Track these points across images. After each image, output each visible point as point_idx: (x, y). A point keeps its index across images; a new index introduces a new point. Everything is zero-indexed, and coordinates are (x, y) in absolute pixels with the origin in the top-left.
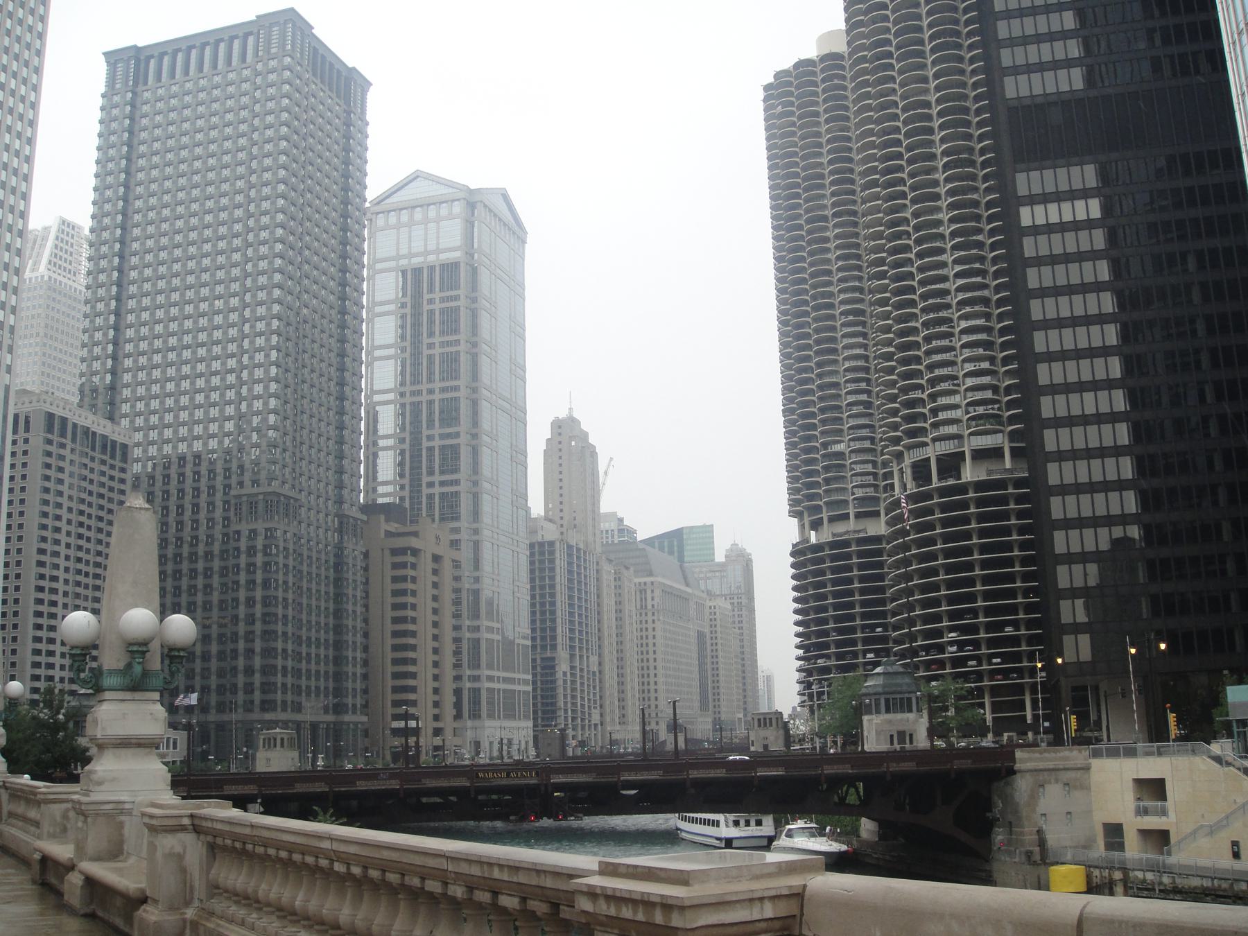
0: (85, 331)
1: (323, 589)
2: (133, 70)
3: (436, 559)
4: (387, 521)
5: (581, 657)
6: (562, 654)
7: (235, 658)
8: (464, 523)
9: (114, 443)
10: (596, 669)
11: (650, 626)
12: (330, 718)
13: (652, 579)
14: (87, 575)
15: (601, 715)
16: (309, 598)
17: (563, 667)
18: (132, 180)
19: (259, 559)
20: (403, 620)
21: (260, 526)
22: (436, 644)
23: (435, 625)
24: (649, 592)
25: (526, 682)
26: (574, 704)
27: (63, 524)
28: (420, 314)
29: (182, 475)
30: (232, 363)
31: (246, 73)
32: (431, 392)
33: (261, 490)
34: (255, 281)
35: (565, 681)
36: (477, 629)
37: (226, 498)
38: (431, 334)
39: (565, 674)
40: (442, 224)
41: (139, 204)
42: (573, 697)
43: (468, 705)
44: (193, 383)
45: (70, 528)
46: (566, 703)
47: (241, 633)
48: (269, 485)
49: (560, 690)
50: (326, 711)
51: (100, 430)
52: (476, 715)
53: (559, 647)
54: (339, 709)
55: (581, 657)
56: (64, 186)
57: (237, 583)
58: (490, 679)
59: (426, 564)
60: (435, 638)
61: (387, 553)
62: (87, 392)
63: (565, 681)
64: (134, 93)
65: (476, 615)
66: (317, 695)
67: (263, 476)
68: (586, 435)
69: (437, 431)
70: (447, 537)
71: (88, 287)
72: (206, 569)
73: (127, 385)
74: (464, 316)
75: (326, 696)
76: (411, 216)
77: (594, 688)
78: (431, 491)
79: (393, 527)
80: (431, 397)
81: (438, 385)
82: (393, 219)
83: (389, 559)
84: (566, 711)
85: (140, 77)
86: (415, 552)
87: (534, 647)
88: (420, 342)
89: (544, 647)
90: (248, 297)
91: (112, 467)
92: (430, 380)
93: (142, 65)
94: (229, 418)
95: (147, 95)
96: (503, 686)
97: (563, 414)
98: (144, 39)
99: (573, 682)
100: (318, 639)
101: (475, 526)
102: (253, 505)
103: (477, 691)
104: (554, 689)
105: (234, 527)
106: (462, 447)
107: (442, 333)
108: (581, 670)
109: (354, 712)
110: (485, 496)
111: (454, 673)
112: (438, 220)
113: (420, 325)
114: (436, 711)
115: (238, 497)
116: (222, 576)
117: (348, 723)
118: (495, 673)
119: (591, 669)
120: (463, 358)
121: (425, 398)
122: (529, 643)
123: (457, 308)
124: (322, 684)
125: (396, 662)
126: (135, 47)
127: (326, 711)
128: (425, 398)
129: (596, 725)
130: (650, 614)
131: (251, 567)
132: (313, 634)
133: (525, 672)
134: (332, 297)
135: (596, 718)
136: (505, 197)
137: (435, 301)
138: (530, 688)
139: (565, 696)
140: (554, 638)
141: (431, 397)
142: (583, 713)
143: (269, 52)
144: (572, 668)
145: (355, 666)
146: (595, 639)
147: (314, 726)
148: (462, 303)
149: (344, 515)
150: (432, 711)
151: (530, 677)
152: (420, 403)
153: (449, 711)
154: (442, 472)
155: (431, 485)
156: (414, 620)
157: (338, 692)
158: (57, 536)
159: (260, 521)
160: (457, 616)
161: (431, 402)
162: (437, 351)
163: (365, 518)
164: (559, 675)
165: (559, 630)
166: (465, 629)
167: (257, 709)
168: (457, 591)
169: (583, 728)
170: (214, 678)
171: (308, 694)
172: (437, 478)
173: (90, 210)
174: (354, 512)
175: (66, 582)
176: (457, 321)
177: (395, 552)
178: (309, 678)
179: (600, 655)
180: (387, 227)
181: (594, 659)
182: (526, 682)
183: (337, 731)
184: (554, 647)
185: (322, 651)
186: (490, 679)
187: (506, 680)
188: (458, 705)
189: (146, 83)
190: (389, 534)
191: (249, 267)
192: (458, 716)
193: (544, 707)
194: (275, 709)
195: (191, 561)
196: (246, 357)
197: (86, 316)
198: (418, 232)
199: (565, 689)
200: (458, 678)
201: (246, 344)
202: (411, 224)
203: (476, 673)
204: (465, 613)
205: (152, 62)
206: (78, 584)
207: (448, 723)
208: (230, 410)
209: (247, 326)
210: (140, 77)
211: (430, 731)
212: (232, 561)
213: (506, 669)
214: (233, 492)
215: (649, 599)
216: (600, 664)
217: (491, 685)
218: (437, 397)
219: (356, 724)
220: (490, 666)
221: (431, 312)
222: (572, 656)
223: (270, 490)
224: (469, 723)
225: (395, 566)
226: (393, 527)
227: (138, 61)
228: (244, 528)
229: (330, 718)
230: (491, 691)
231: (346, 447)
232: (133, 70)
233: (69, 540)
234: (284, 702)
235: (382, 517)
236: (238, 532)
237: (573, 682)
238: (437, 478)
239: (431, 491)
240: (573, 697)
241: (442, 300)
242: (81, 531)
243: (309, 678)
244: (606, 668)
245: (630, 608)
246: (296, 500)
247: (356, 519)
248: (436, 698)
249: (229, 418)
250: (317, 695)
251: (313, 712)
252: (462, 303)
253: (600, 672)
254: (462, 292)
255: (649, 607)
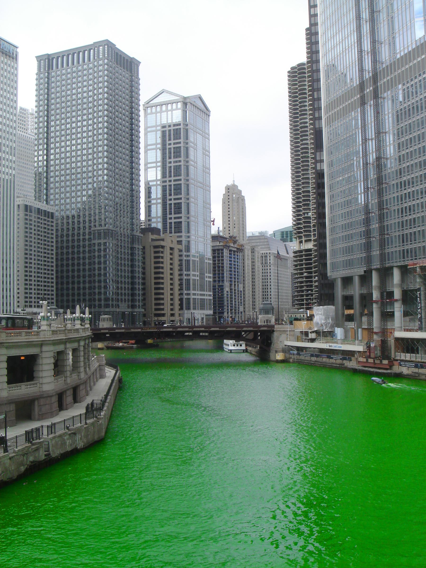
0: (36, 140)
1: (126, 245)
2: (48, 63)
3: (172, 249)
4: (152, 234)
5: (235, 285)
6: (226, 284)
7: (95, 289)
8: (183, 234)
9: (49, 212)
10: (242, 289)
11: (269, 271)
12: (130, 310)
13: (269, 251)
14: (41, 252)
15: (244, 308)
16: (121, 254)
17: (227, 289)
18: (50, 76)
19: (102, 253)
20: (158, 257)
21: (102, 241)
22: (172, 282)
23: (171, 264)
24: (268, 257)
25: (210, 295)
26: (231, 304)
27: (33, 244)
28: (166, 149)
29: (73, 222)
30: (90, 180)
31: (91, 65)
32: (170, 181)
33: (102, 228)
34: (98, 114)
35: (227, 295)
36: (188, 275)
37: (90, 231)
38: (170, 195)
39: (227, 292)
40: (174, 112)
41: (53, 96)
42: (231, 301)
43: (185, 304)
44: (76, 188)
45: (35, 245)
46: (228, 304)
47: (96, 249)
48: (105, 226)
49: (225, 299)
50: (128, 308)
51: (44, 209)
52: (188, 308)
53: (225, 282)
54: (133, 307)
55: (235, 285)
56: (27, 97)
57: (94, 256)
58: (194, 294)
59: (167, 251)
60: (171, 279)
61: (152, 247)
62: (37, 174)
63: (227, 295)
64: (48, 73)
65: (188, 269)
66: (125, 302)
67: (103, 223)
68: (240, 192)
69: (172, 142)
70: (175, 240)
71: (36, 112)
72: (83, 245)
73: (52, 171)
74: (184, 225)
75: (128, 302)
76: (161, 109)
77: (241, 297)
78: (171, 221)
79: (155, 237)
80: (170, 128)
81: (173, 178)
82: (154, 109)
83: (153, 250)
84: (228, 307)
85: (50, 67)
86: (163, 247)
87: (214, 281)
88: (166, 161)
89: (219, 281)
90: (95, 115)
91: (48, 221)
92: (170, 176)
93: (51, 62)
94: (90, 189)
95: (53, 74)
96: (200, 297)
97: (230, 183)
98: (52, 50)
99: (231, 295)
100: (125, 282)
101: (188, 235)
102: (99, 234)
103: (188, 299)
104: (223, 301)
105: (93, 242)
106: (183, 204)
107: (174, 157)
108: (235, 290)
109: (139, 308)
110: (192, 223)
111: (179, 273)
112: (172, 110)
113: (166, 154)
114: (172, 307)
115: (94, 230)
116: (89, 247)
117: (136, 312)
118: (196, 292)
119: (240, 290)
120: (183, 224)
121: (168, 184)
122: (211, 262)
123: (180, 147)
124: (127, 298)
125: (156, 283)
126: (48, 54)
127: (128, 308)
128: (168, 184)
129: (241, 312)
130: (268, 266)
131: (100, 269)
132: (123, 256)
133: (210, 291)
134: (127, 146)
135: (241, 309)
136: (200, 98)
137: (171, 144)
138: (212, 298)
139: (228, 301)
140: (223, 277)
141: (170, 128)
142: (235, 307)
143: (99, 57)
144: (231, 289)
145: (139, 285)
146: (241, 278)
147: (123, 313)
148: (182, 182)
149: (134, 235)
150: (170, 312)
151: (211, 293)
152: (166, 186)
153: (177, 307)
154: (174, 176)
155: (171, 218)
156: (162, 257)
157: (133, 300)
158: (31, 248)
159: (102, 239)
160: (181, 270)
161: (170, 186)
162: (172, 165)
163: (142, 235)
164: (225, 293)
165: (225, 274)
166: (184, 256)
167: (103, 307)
168: (181, 260)
169: (235, 313)
170: (87, 296)
171: (122, 301)
172: (173, 197)
173: (35, 104)
174: (138, 234)
175: (35, 255)
176: (180, 152)
177: (155, 247)
178: (121, 272)
179: (244, 284)
180: (152, 113)
181: (241, 286)
182: (210, 295)
183: (132, 315)
184: (223, 281)
185: (127, 286)
186: (194, 294)
187: (201, 295)
188: (181, 305)
189: (52, 69)
190: (153, 240)
191: (96, 69)
192: (181, 309)
193: (218, 303)
194: (109, 307)
195: (78, 254)
196: (95, 131)
197: (36, 134)
198: (164, 115)
199: (227, 298)
200: (181, 294)
201: (95, 92)
202: (161, 111)
203: (188, 273)
204: (184, 269)
205: (55, 59)
206: (39, 247)
207: (177, 311)
208: (90, 186)
209: (95, 96)
210: (50, 67)
211: (169, 314)
212: (92, 254)
213: (201, 290)
214: (92, 229)
215: (268, 260)
216: (244, 287)
217: (194, 297)
218: (173, 183)
219: (140, 312)
220: (194, 289)
221: (171, 223)
222: (231, 285)
223: (105, 228)
224: (186, 311)
225: (155, 252)
226: (155, 237)
227: (49, 60)
228: (96, 242)
229: (130, 310)
230: (194, 280)
231: (134, 198)
232: (48, 63)
233: (35, 245)
234: (112, 305)
235: (150, 233)
236: (94, 244)
237: (231, 295)
238: (173, 197)
239: (171, 221)
240: (231, 301)
241: (174, 144)
242: (39, 245)
243: (121, 272)
244: (246, 289)
245: (258, 264)
246: (115, 231)
247: (139, 236)
248: (172, 302)
249: (90, 189)
250: (125, 302)
251: (124, 308)
252: (183, 201)
253: (244, 291)
254: (182, 196)
255: (268, 263)
